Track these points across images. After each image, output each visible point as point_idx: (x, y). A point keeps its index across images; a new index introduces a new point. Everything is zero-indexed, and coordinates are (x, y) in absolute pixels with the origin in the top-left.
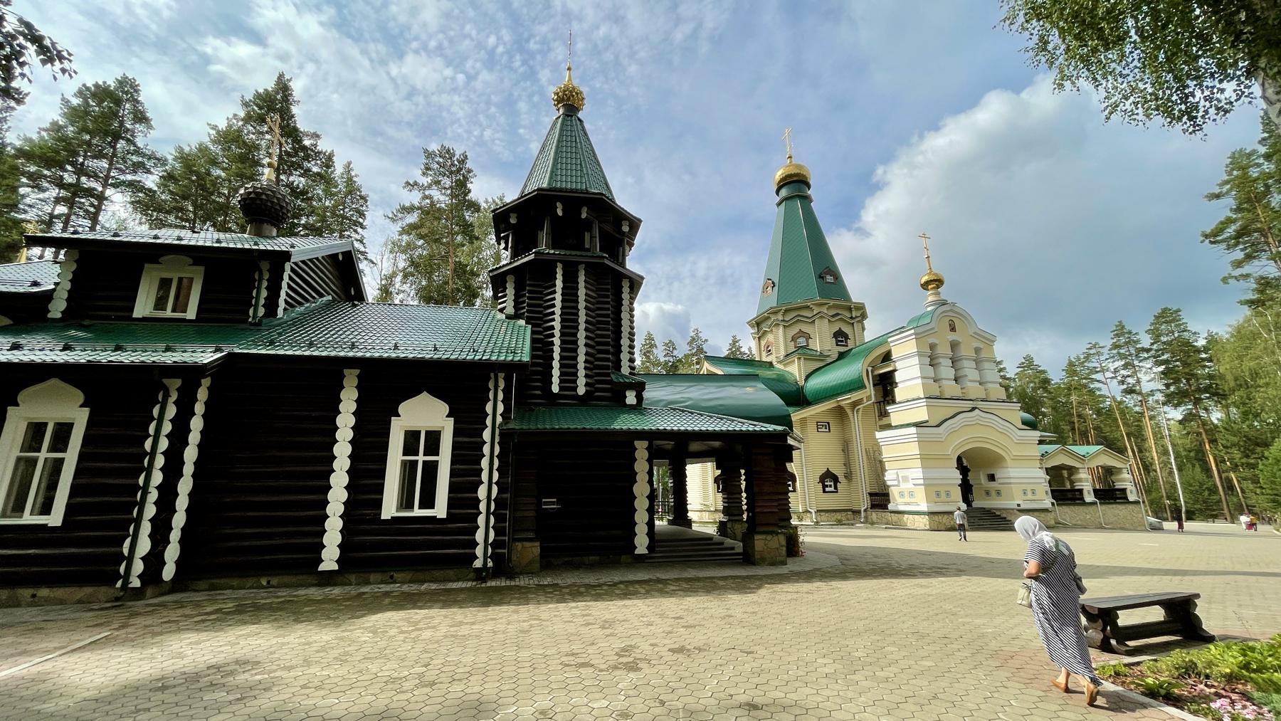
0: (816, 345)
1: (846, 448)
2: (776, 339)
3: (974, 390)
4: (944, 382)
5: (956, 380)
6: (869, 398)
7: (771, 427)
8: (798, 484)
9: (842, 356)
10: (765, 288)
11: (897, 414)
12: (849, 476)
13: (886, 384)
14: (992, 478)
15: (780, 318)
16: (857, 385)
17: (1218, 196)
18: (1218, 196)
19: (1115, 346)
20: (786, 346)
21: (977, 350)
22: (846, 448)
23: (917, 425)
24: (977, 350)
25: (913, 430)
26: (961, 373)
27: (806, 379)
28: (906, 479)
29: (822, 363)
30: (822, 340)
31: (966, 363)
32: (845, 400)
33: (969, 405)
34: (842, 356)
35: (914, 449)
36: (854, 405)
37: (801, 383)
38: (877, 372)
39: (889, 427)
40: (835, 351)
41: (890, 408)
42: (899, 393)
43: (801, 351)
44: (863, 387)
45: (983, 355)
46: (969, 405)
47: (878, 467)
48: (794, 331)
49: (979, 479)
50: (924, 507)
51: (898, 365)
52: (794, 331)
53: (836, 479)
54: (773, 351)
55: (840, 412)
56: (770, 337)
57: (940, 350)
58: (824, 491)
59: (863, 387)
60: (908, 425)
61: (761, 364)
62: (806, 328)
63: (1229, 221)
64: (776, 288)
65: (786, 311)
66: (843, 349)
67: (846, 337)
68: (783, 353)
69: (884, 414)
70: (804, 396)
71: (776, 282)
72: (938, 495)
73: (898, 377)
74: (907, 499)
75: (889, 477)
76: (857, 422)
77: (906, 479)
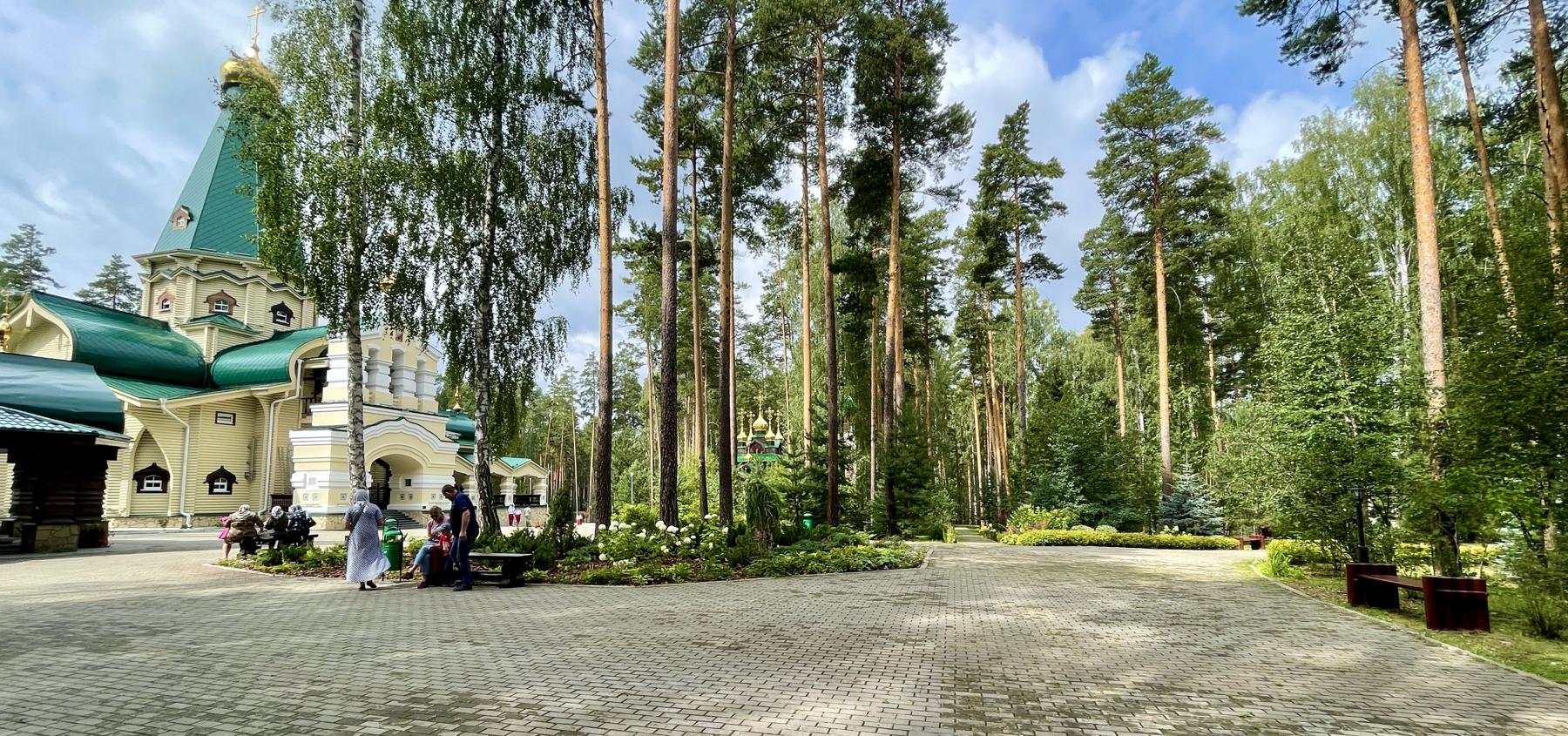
0: (243, 315)
1: (254, 446)
2: (181, 292)
3: (407, 399)
4: (378, 389)
5: (392, 389)
6: (292, 393)
7: (76, 428)
8: (171, 484)
9: (278, 336)
10: (176, 217)
11: (319, 414)
12: (250, 476)
13: (316, 380)
14: (408, 483)
15: (193, 267)
16: (281, 376)
17: (629, 282)
18: (629, 282)
19: (585, 373)
20: (195, 307)
21: (420, 364)
22: (254, 446)
23: (334, 429)
24: (420, 364)
25: (329, 433)
26: (397, 383)
27: (217, 356)
28: (313, 481)
29: (249, 340)
30: (253, 308)
31: (406, 374)
32: (261, 391)
33: (397, 414)
34: (278, 336)
35: (327, 452)
36: (273, 398)
37: (209, 359)
38: (308, 366)
39: (308, 426)
40: (270, 328)
41: (313, 407)
42: (327, 393)
43: (220, 313)
44: (288, 379)
45: (426, 368)
46: (397, 414)
47: (286, 468)
48: (213, 289)
49: (397, 484)
50: (324, 510)
51: (332, 364)
52: (213, 289)
53: (231, 479)
54: (173, 307)
55: (253, 405)
56: (171, 289)
57: (379, 357)
58: (211, 492)
59: (288, 379)
60: (324, 428)
61: (148, 323)
62: (231, 291)
63: (629, 303)
64: (194, 225)
65: (204, 261)
66: (281, 328)
67: (290, 314)
68: (187, 315)
69: (307, 413)
70: (210, 377)
71: (197, 214)
72: (343, 497)
73: (330, 376)
74: (310, 501)
75: (296, 479)
76: (272, 417)
77: (313, 481)
